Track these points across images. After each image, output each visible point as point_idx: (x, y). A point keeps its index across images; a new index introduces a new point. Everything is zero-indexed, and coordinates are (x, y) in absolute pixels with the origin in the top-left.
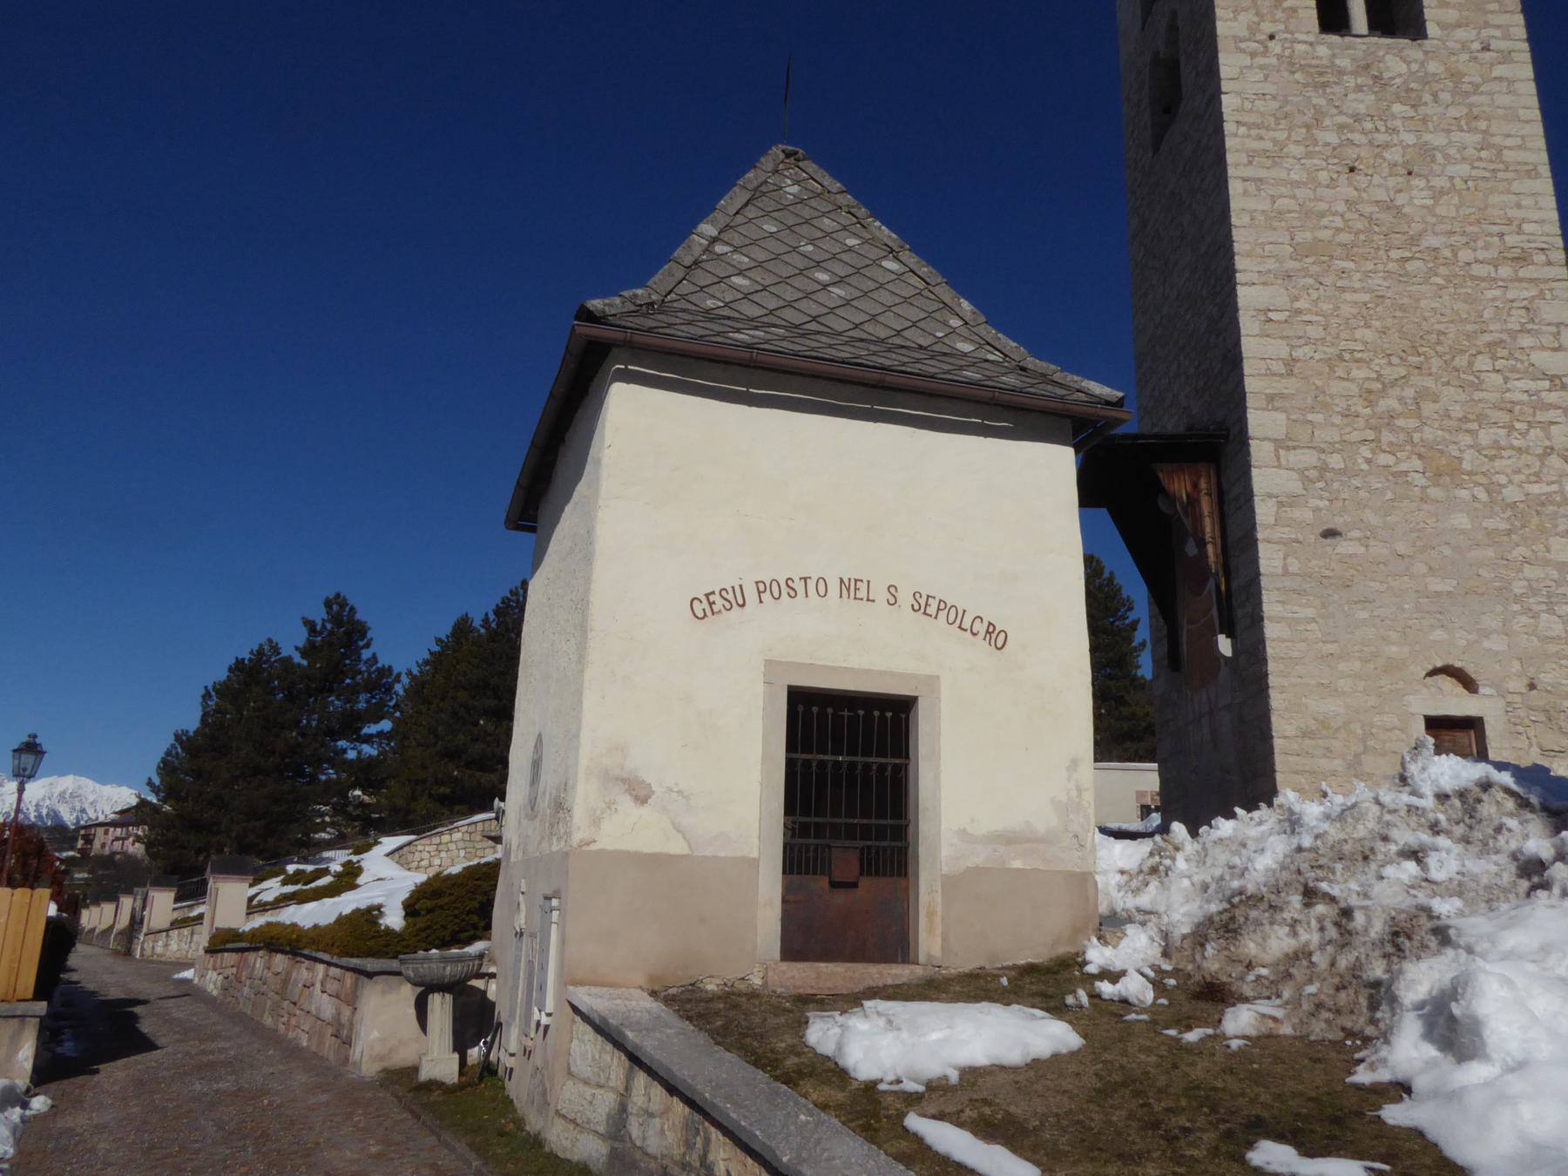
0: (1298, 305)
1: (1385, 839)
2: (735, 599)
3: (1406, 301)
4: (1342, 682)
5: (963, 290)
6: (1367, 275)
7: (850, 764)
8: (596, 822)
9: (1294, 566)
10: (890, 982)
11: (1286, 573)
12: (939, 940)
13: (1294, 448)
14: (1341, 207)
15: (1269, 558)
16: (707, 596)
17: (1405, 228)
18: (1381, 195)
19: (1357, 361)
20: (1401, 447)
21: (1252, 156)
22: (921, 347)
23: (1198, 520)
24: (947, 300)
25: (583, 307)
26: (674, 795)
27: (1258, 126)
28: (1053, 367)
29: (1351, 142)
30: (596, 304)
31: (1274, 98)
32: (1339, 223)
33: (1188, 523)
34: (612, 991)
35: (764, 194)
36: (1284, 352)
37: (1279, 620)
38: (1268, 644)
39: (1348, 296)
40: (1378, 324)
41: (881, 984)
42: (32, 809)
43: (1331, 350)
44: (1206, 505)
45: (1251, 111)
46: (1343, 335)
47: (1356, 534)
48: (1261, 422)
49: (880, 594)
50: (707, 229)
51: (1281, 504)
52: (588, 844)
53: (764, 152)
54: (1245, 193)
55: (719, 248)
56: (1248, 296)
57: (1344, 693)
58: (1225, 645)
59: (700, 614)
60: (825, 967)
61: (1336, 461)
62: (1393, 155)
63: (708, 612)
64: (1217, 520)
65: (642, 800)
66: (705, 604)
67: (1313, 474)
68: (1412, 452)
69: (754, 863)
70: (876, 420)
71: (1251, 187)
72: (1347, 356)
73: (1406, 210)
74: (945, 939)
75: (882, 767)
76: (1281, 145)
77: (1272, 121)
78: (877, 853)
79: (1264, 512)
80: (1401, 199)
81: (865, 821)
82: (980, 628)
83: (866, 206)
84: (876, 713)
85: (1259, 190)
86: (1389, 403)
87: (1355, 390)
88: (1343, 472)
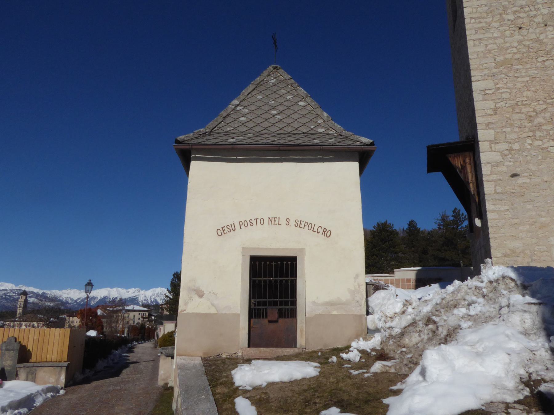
0: (498, 86)
1: (464, 300)
3: (545, 78)
4: (521, 234)
5: (324, 108)
6: (528, 69)
7: (273, 283)
8: (186, 304)
9: (499, 189)
10: (286, 354)
11: (496, 193)
12: (305, 339)
13: (498, 143)
14: (516, 44)
15: (488, 188)
16: (222, 228)
17: (544, 48)
18: (534, 36)
19: (525, 105)
20: (545, 137)
21: (477, 30)
23: (466, 174)
24: (319, 113)
27: (479, 18)
28: (351, 133)
29: (520, 17)
30: (181, 138)
31: (486, 6)
32: (515, 50)
33: (462, 176)
34: (190, 358)
35: (261, 85)
36: (493, 105)
37: (493, 211)
38: (489, 221)
39: (519, 79)
40: (533, 89)
43: (513, 102)
44: (469, 168)
45: (476, 12)
46: (518, 95)
47: (526, 174)
48: (483, 134)
49: (283, 222)
50: (235, 102)
51: (493, 166)
52: (183, 311)
53: (265, 69)
54: (474, 45)
55: (238, 108)
56: (476, 86)
57: (522, 239)
58: (478, 222)
59: (220, 234)
60: (262, 349)
61: (516, 146)
62: (539, 19)
64: (474, 173)
65: (201, 296)
66: (222, 231)
67: (507, 152)
68: (550, 139)
69: (239, 315)
70: (282, 162)
71: (477, 43)
72: (520, 103)
73: (545, 40)
74: (307, 339)
75: (287, 281)
76: (489, 24)
77: (485, 15)
79: (485, 170)
80: (542, 37)
81: (281, 300)
83: (297, 82)
84: (285, 263)
85: (480, 43)
86: (540, 120)
87: (523, 116)
88: (520, 150)
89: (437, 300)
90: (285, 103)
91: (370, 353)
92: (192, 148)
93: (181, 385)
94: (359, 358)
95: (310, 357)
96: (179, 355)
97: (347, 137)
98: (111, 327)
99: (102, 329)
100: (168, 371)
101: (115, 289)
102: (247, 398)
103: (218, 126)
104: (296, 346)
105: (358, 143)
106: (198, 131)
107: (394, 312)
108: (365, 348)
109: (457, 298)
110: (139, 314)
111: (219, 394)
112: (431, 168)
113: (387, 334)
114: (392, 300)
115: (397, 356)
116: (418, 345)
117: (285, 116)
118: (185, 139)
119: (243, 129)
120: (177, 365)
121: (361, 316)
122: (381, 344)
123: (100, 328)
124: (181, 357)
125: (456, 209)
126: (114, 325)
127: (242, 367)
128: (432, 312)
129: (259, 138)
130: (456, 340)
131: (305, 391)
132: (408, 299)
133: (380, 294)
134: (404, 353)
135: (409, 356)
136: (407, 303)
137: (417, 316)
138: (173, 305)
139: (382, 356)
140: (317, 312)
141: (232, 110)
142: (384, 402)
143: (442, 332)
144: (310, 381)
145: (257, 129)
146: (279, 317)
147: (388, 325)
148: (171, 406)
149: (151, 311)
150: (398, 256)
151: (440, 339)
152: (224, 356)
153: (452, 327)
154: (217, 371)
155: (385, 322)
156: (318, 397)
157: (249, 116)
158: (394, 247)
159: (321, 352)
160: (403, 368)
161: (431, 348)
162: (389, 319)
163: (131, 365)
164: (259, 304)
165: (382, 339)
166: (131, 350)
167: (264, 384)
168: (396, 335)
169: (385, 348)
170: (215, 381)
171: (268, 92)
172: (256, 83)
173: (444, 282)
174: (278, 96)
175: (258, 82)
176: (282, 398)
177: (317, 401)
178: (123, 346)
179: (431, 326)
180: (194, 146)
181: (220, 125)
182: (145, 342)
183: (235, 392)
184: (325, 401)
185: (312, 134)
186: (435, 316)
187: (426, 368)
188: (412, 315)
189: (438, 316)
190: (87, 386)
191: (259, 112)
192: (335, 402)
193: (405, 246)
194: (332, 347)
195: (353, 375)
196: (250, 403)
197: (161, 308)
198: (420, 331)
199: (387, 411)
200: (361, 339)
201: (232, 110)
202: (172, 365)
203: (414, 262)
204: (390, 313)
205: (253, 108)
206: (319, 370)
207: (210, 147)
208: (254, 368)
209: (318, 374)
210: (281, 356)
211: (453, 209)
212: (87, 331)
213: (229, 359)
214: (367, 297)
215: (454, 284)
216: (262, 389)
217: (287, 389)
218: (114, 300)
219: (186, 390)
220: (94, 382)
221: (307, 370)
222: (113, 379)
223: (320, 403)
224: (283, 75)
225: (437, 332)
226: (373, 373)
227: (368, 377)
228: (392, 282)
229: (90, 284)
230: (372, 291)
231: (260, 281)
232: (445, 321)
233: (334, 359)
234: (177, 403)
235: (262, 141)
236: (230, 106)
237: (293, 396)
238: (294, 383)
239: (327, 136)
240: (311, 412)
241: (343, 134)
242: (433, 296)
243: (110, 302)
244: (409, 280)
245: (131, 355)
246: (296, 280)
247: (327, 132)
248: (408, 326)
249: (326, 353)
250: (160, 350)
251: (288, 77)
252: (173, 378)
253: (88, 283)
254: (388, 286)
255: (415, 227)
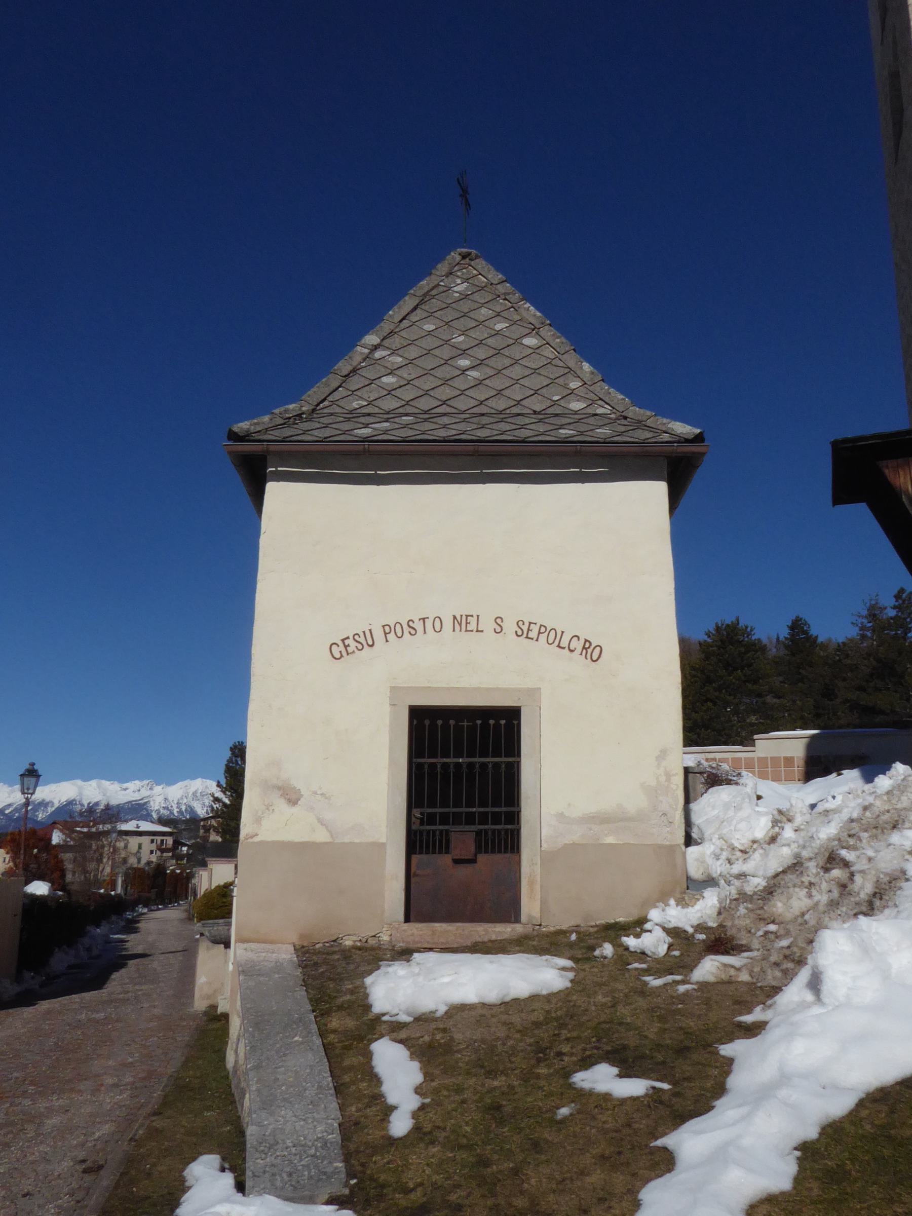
2: (366, 641)
7: (463, 768)
8: (258, 820)
10: (494, 938)
16: (343, 640)
22: (535, 412)
24: (572, 364)
25: (230, 430)
26: (319, 797)
28: (649, 413)
30: (242, 426)
35: (433, 297)
41: (486, 939)
42: (175, 806)
49: (487, 624)
50: (372, 339)
52: (252, 837)
53: (440, 259)
55: (378, 354)
59: (338, 656)
60: (439, 926)
63: (344, 653)
69: (381, 847)
74: (544, 902)
75: (496, 765)
78: (434, 835)
81: (482, 810)
82: (577, 645)
83: (520, 291)
84: (492, 722)
89: (853, 809)
90: (490, 341)
91: (693, 936)
92: (268, 452)
93: (245, 1013)
94: (666, 947)
95: (552, 944)
96: (241, 940)
97: (639, 422)
98: (85, 871)
99: (63, 876)
100: (217, 977)
101: (94, 783)
102: (400, 1042)
103: (330, 398)
104: (517, 920)
105: (666, 437)
106: (282, 409)
107: (751, 838)
108: (680, 925)
109: (899, 806)
110: (152, 841)
111: (334, 1031)
112: (843, 493)
113: (732, 891)
114: (747, 811)
115: (756, 944)
116: (807, 917)
117: (490, 372)
118: (252, 429)
119: (390, 404)
120: (237, 964)
121: (672, 849)
122: (719, 913)
123: (56, 875)
124: (246, 945)
125: (902, 591)
126: (92, 866)
127: (390, 969)
128: (839, 840)
129: (427, 426)
130: (896, 906)
131: (537, 1025)
132: (784, 806)
133: (720, 795)
134: (772, 937)
135: (785, 943)
136: (782, 817)
137: (804, 847)
138: (229, 817)
139: (720, 942)
140: (568, 840)
141: (364, 360)
142: (722, 1052)
143: (862, 888)
144: (549, 1001)
145: (425, 404)
146: (479, 849)
147: (736, 869)
148: (223, 1059)
149: (180, 832)
150: (764, 703)
151: (857, 904)
152: (348, 943)
153: (886, 874)
154: (331, 976)
155: (730, 862)
156: (568, 1039)
157: (404, 373)
158: (755, 682)
159: (578, 933)
160: (769, 971)
161: (834, 924)
162: (739, 854)
163: (131, 962)
164: (430, 819)
165: (720, 903)
166: (131, 927)
167: (442, 1009)
168: (755, 893)
169: (728, 924)
170: (327, 1002)
171: (449, 315)
172: (420, 293)
173: (872, 765)
174: (474, 324)
175: (426, 289)
176: (483, 1041)
177: (566, 1049)
178: (114, 918)
179: (836, 873)
180: (274, 447)
181: (336, 396)
182: (165, 908)
183: (374, 1026)
184: (584, 1050)
185: (557, 415)
186: (847, 848)
187: (821, 973)
188: (794, 846)
189: (855, 848)
190: (27, 1012)
191: (429, 363)
192: (608, 1052)
193: (781, 679)
194: (603, 922)
195: (652, 988)
196: (407, 1053)
197: (204, 826)
198: (811, 884)
199: (728, 1073)
200: (672, 902)
201: (364, 360)
202: (226, 962)
203: (802, 718)
204: (740, 840)
205: (413, 352)
206: (571, 975)
207: (313, 448)
208: (417, 970)
209: (569, 985)
210: (483, 943)
211: (895, 591)
212: (27, 883)
213: (360, 949)
214: (688, 800)
215: (893, 772)
216: (436, 1020)
217: (494, 1020)
218: (91, 809)
219: (258, 1022)
220: (43, 1002)
221: (545, 976)
222: (87, 996)
223: (572, 1054)
224: (486, 273)
225: (850, 887)
226: (697, 983)
227: (686, 993)
228: (749, 766)
229: (31, 775)
230: (700, 787)
231: (433, 766)
232: (870, 859)
233: (608, 949)
234: (236, 1052)
235: (434, 433)
236: (359, 348)
237: (508, 1037)
238: (516, 1004)
239: (591, 420)
240: (551, 1075)
241: (630, 415)
242: (843, 801)
243: (81, 814)
244: (789, 761)
245: (132, 936)
246: (519, 763)
247: (590, 411)
248: (784, 872)
249: (590, 935)
250: (198, 926)
251: (496, 276)
252: (227, 992)
253: (28, 770)
254: (739, 774)
255: (806, 633)
